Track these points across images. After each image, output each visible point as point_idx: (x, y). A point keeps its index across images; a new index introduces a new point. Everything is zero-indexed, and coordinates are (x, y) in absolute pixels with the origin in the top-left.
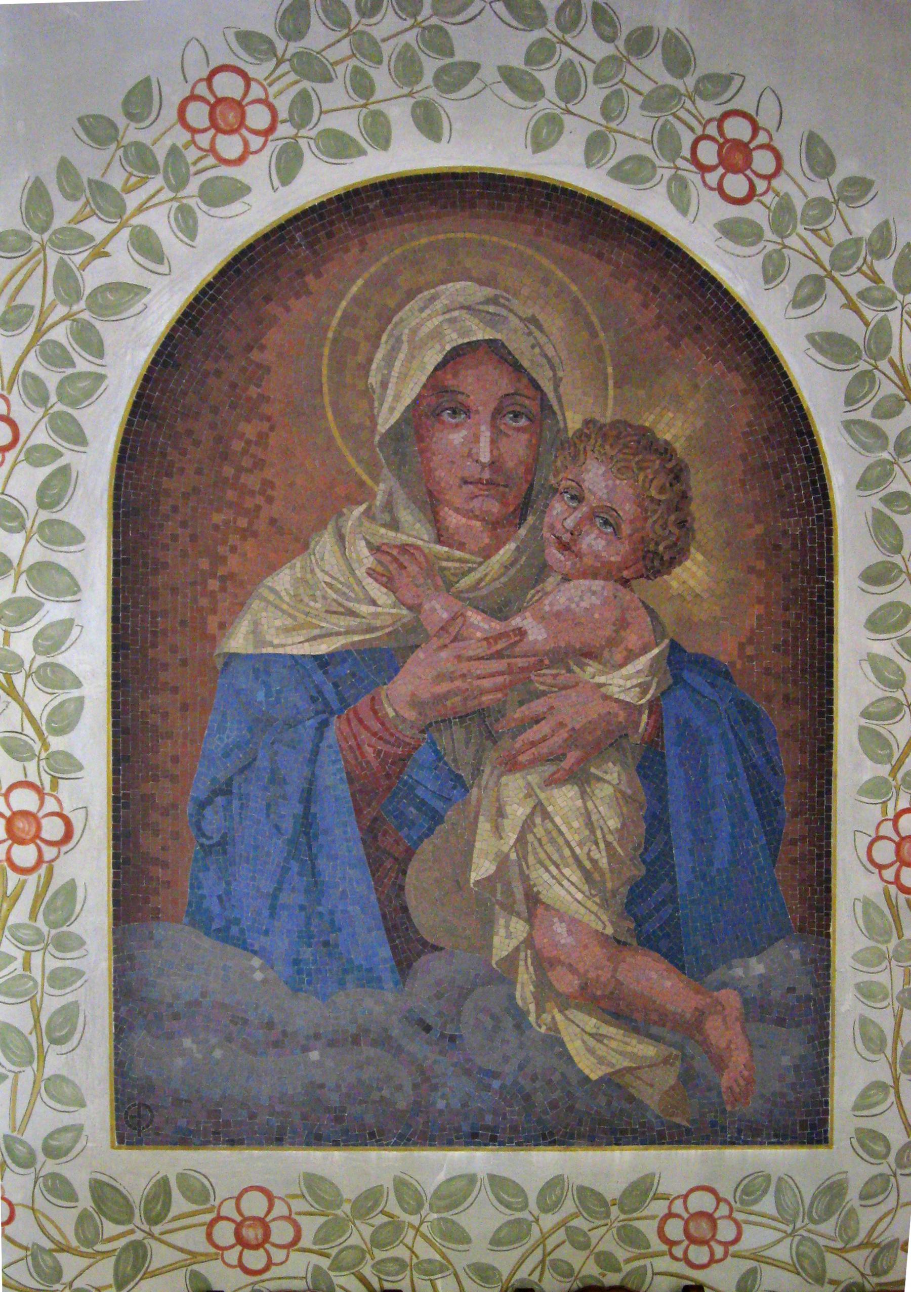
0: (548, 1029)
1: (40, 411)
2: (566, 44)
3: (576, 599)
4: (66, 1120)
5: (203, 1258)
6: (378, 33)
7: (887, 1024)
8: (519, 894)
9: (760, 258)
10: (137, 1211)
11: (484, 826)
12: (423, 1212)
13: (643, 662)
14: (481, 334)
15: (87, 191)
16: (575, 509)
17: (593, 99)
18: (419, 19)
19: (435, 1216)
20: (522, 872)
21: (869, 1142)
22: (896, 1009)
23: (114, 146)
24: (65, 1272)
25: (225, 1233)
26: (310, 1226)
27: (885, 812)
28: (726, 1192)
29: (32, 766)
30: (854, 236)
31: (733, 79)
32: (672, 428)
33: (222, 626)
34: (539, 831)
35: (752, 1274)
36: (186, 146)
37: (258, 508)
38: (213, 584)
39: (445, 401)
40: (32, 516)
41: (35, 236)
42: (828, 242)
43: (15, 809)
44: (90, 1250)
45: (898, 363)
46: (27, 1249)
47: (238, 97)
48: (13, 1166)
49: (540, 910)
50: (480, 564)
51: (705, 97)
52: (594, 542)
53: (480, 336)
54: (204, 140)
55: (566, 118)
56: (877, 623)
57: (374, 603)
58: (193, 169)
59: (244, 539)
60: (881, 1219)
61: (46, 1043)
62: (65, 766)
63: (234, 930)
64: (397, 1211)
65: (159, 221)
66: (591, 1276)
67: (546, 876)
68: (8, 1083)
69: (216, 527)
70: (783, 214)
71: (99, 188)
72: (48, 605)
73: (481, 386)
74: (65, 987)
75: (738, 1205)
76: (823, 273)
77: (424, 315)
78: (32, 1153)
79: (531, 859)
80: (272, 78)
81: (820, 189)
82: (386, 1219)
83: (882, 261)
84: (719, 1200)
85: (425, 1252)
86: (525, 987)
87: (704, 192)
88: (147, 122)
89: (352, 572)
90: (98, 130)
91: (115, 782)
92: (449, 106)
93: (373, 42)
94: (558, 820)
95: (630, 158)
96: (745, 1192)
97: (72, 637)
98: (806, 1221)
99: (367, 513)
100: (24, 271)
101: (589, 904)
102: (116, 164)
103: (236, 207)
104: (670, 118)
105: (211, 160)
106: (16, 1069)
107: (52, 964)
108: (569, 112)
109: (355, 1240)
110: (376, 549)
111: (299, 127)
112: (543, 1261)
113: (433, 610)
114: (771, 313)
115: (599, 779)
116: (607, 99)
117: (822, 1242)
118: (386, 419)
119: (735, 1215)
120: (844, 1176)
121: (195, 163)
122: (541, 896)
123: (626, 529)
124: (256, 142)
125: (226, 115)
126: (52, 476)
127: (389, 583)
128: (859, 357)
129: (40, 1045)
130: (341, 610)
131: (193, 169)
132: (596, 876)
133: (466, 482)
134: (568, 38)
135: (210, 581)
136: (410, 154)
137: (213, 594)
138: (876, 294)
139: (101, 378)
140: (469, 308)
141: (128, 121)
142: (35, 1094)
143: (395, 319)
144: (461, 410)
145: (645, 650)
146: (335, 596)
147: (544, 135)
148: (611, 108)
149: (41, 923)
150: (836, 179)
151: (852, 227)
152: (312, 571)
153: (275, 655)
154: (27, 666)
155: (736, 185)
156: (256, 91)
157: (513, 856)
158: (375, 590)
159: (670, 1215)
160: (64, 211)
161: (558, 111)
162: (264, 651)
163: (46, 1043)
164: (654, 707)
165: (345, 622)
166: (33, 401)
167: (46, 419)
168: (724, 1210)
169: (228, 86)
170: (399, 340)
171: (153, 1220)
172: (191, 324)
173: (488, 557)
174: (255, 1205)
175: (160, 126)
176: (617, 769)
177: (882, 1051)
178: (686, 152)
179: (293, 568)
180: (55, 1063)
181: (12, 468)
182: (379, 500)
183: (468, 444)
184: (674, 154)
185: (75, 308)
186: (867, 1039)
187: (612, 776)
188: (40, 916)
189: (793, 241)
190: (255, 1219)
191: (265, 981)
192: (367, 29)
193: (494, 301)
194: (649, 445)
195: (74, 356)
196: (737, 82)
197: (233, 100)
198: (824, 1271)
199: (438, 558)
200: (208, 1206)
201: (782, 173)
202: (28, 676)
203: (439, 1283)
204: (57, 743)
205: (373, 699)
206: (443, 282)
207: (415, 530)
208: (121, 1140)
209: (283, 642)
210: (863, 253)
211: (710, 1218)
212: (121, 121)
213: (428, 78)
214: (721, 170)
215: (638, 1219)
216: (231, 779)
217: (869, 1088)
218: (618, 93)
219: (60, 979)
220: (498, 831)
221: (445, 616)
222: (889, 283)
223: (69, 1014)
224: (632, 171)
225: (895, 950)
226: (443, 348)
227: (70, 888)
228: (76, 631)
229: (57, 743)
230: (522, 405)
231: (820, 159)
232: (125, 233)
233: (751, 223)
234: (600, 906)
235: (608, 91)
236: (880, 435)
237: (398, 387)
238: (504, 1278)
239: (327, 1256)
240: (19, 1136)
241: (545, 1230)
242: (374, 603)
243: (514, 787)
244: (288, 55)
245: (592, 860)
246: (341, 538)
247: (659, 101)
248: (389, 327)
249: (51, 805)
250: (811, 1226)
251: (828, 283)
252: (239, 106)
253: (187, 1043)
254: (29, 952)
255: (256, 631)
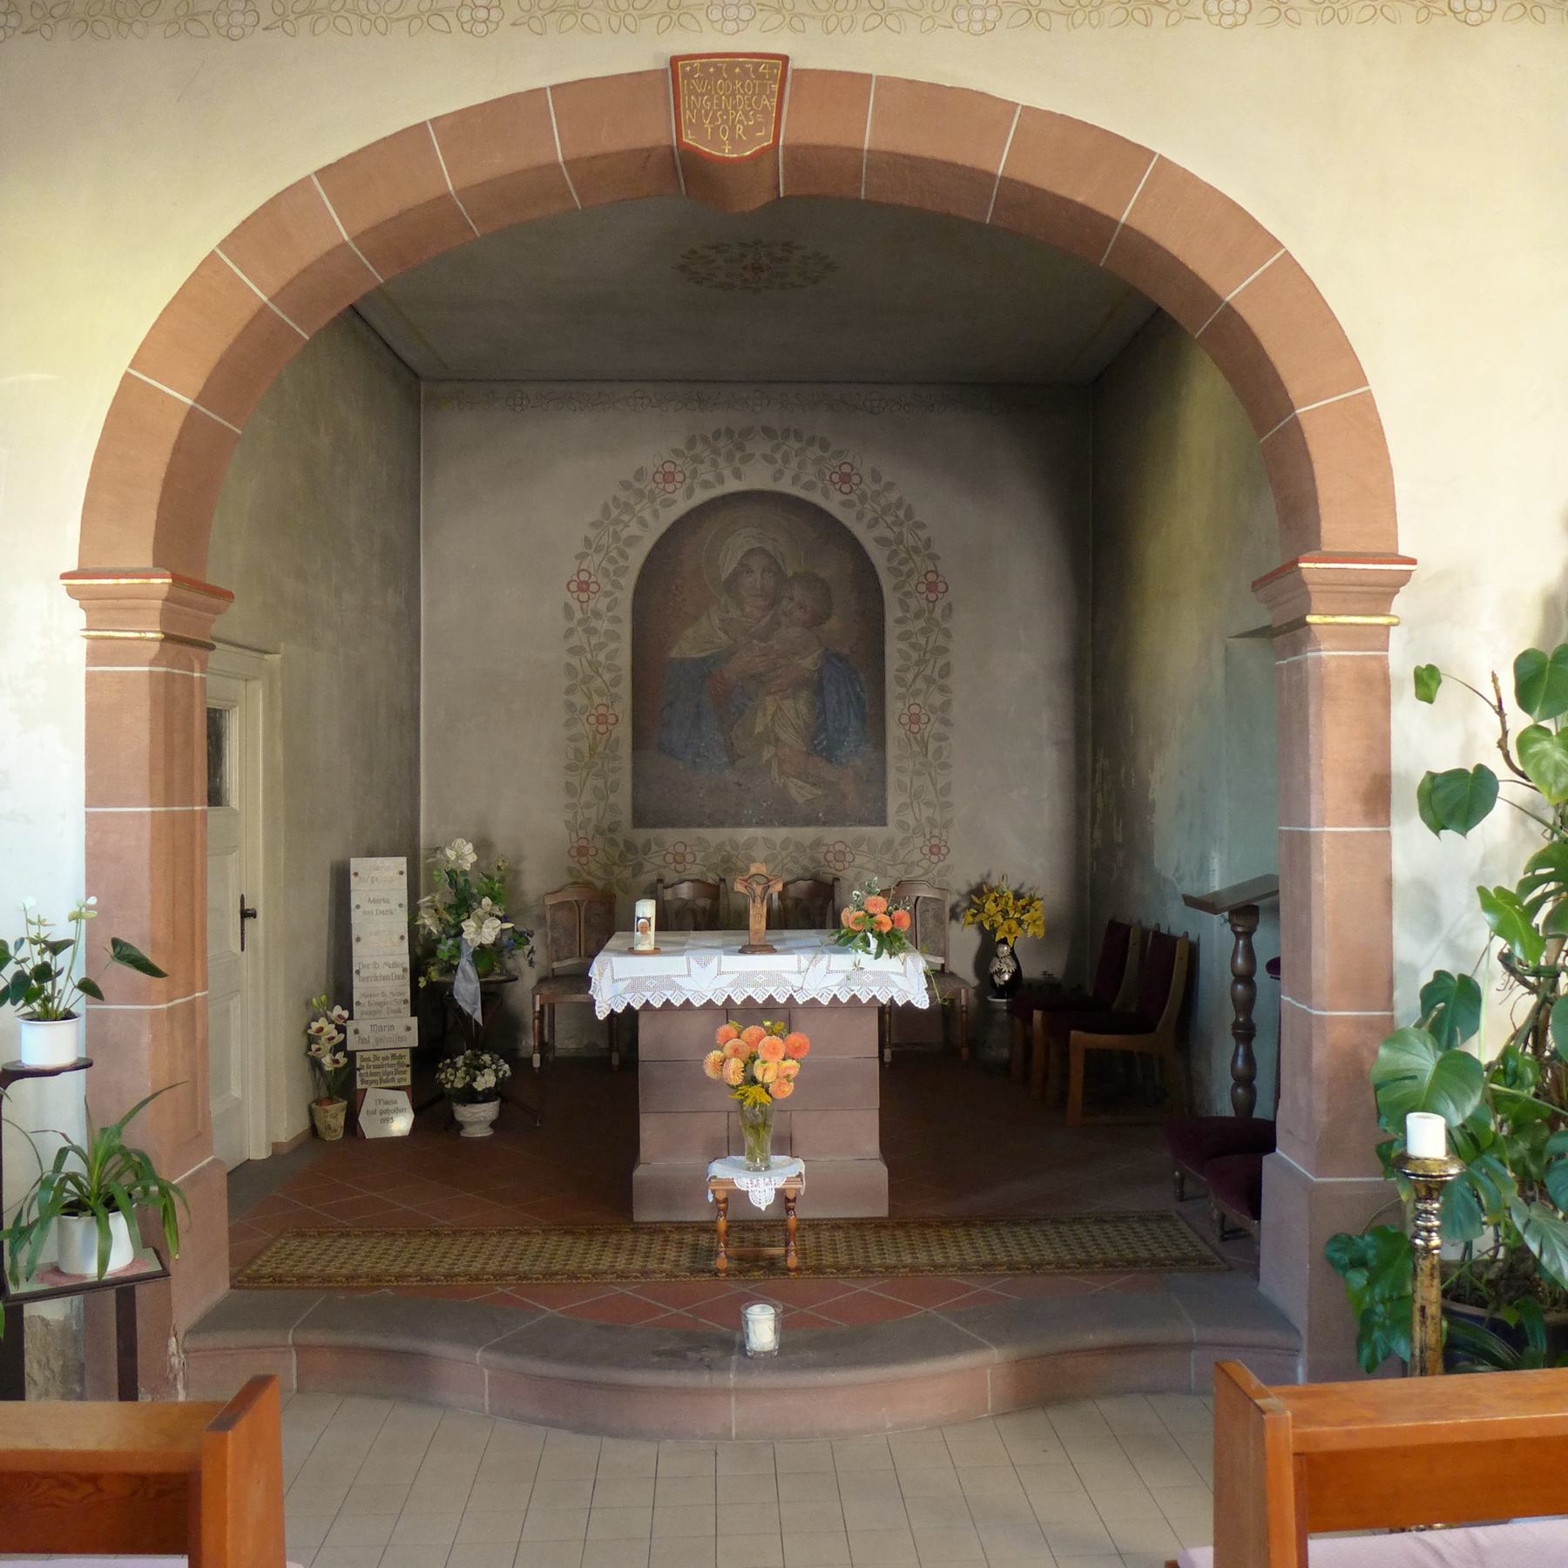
11: (760, 714)
14: (757, 545)
17: (794, 464)
21: (902, 825)
25: (670, 858)
26: (699, 856)
56: (901, 638)
62: (615, 698)
65: (647, 515)
71: (626, 504)
73: (757, 563)
81: (876, 487)
86: (775, 772)
90: (626, 485)
110: (721, 620)
118: (724, 576)
125: (668, 477)
127: (726, 632)
144: (750, 571)
147: (778, 476)
148: (801, 465)
153: (224, 1464)
155: (846, 488)
158: (722, 634)
160: (615, 513)
169: (669, 467)
174: (680, 848)
180: (612, 798)
187: (805, 694)
224: (810, 486)
231: (876, 477)
243: (769, 698)
247: (817, 461)
252: (672, 473)
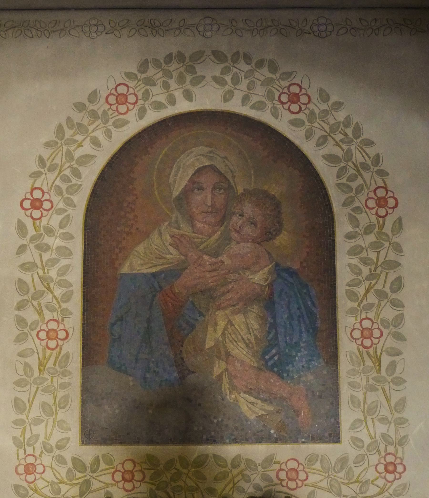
0: (234, 401)
1: (60, 197)
2: (234, 67)
3: (242, 250)
4: (65, 436)
5: (110, 486)
6: (171, 69)
7: (361, 398)
8: (223, 353)
9: (304, 131)
10: (88, 468)
12: (189, 469)
13: (266, 270)
15: (76, 126)
16: (240, 219)
18: (185, 63)
19: (193, 470)
20: (224, 344)
21: (356, 442)
22: (364, 391)
23: (85, 111)
24: (62, 490)
27: (356, 320)
28: (302, 461)
29: (55, 314)
30: (337, 121)
31: (292, 73)
32: (275, 190)
33: (120, 264)
34: (230, 330)
35: (313, 492)
36: (108, 110)
37: (132, 225)
38: (117, 251)
39: (195, 186)
40: (57, 231)
41: (59, 141)
42: (328, 124)
43: (49, 328)
44: (71, 483)
45: (355, 163)
46: (49, 482)
47: (125, 93)
48: (45, 452)
49: (230, 358)
50: (208, 239)
51: (283, 80)
52: (248, 230)
53: (207, 164)
54: (114, 107)
55: (235, 91)
57: (172, 254)
58: (110, 117)
59: (127, 235)
60: (362, 472)
61: (58, 408)
63: (123, 368)
64: (180, 469)
65: (100, 135)
66: (251, 493)
67: (232, 346)
68: (45, 423)
69: (118, 232)
70: (312, 116)
72: (62, 260)
73: (207, 180)
74: (65, 388)
75: (307, 466)
76: (327, 134)
77: (188, 158)
78: (52, 447)
79: (227, 340)
80: (137, 85)
81: (324, 107)
82: (176, 471)
83: (348, 129)
84: (299, 464)
85: (190, 483)
87: (283, 111)
88: (96, 103)
89: (164, 244)
90: (80, 107)
91: (83, 318)
92: (196, 91)
93: (169, 71)
94: (236, 326)
95: (257, 102)
96: (309, 461)
97: (70, 270)
98: (333, 472)
99: (169, 224)
100: (56, 152)
101: (248, 355)
102: (86, 117)
103: (125, 128)
104: (271, 88)
105: (116, 113)
106: (48, 418)
107: (61, 381)
108: (236, 89)
109: (164, 479)
110: (172, 236)
111: (145, 101)
112: (233, 487)
113: (192, 255)
114: (308, 148)
115: (251, 311)
116: (249, 83)
117: (339, 480)
119: (306, 470)
120: (347, 455)
121: (111, 115)
122: (231, 353)
123: (259, 225)
124: (131, 107)
125: (121, 99)
126: (64, 218)
128: (341, 162)
129: (56, 410)
130: (160, 257)
131: (110, 117)
132: (250, 345)
133: (203, 212)
134: (235, 65)
135: (116, 249)
136: (183, 106)
137: (117, 254)
138: (346, 140)
139: (81, 185)
140: (203, 155)
141: (89, 103)
142: (54, 426)
143: (178, 160)
144: (201, 189)
145: (266, 266)
146: (158, 253)
149: (57, 367)
150: (330, 103)
151: (337, 118)
152: (151, 245)
153: (138, 273)
154: (54, 280)
155: (295, 108)
156: (131, 91)
157: (221, 339)
158: (172, 250)
159: (281, 470)
160: (68, 133)
161: (232, 89)
162: (134, 272)
163: (58, 408)
164: (270, 285)
165: (162, 261)
166: (59, 195)
167: (62, 200)
168: (301, 467)
169: (122, 90)
170: (179, 167)
171: (94, 471)
172: (110, 166)
173: (211, 237)
175: (100, 104)
176: (257, 307)
177: (359, 407)
178: (277, 98)
179: (144, 244)
181: (51, 216)
182: (173, 219)
183: (203, 199)
184: (273, 99)
185: (72, 163)
186: (353, 403)
188: (57, 364)
189: (316, 125)
190: (129, 471)
191: (133, 385)
192: (167, 68)
193: (211, 152)
194: (267, 195)
195: (72, 179)
196: (295, 73)
197: (124, 94)
198: (341, 491)
199: (194, 238)
200: (113, 466)
201: (311, 102)
202: (55, 284)
203: (195, 495)
204: (64, 306)
205: (171, 287)
206: (194, 147)
207: (186, 229)
208: (83, 443)
209: (140, 269)
210: (341, 127)
211: (296, 471)
212: (87, 103)
213: (188, 82)
214: (289, 103)
215: (268, 471)
216: (123, 316)
217: (355, 421)
218: (253, 82)
219: (63, 386)
220: (215, 330)
221: (196, 257)
222: (351, 136)
223: (66, 398)
225: (363, 370)
226: (194, 169)
227: (67, 356)
228: (71, 268)
229: (64, 306)
230: (222, 186)
232: (89, 138)
233: (300, 120)
234: (252, 356)
235: (248, 81)
236: (350, 188)
237: (179, 182)
238: (219, 493)
239: (154, 485)
240: (48, 442)
241: (234, 475)
242: (172, 254)
244: (141, 79)
245: (249, 340)
246: (160, 234)
247: (268, 82)
248: (176, 163)
249: (61, 327)
250: (335, 474)
251: (329, 138)
252: (125, 96)
253: (107, 408)
254: (53, 377)
255: (131, 265)
